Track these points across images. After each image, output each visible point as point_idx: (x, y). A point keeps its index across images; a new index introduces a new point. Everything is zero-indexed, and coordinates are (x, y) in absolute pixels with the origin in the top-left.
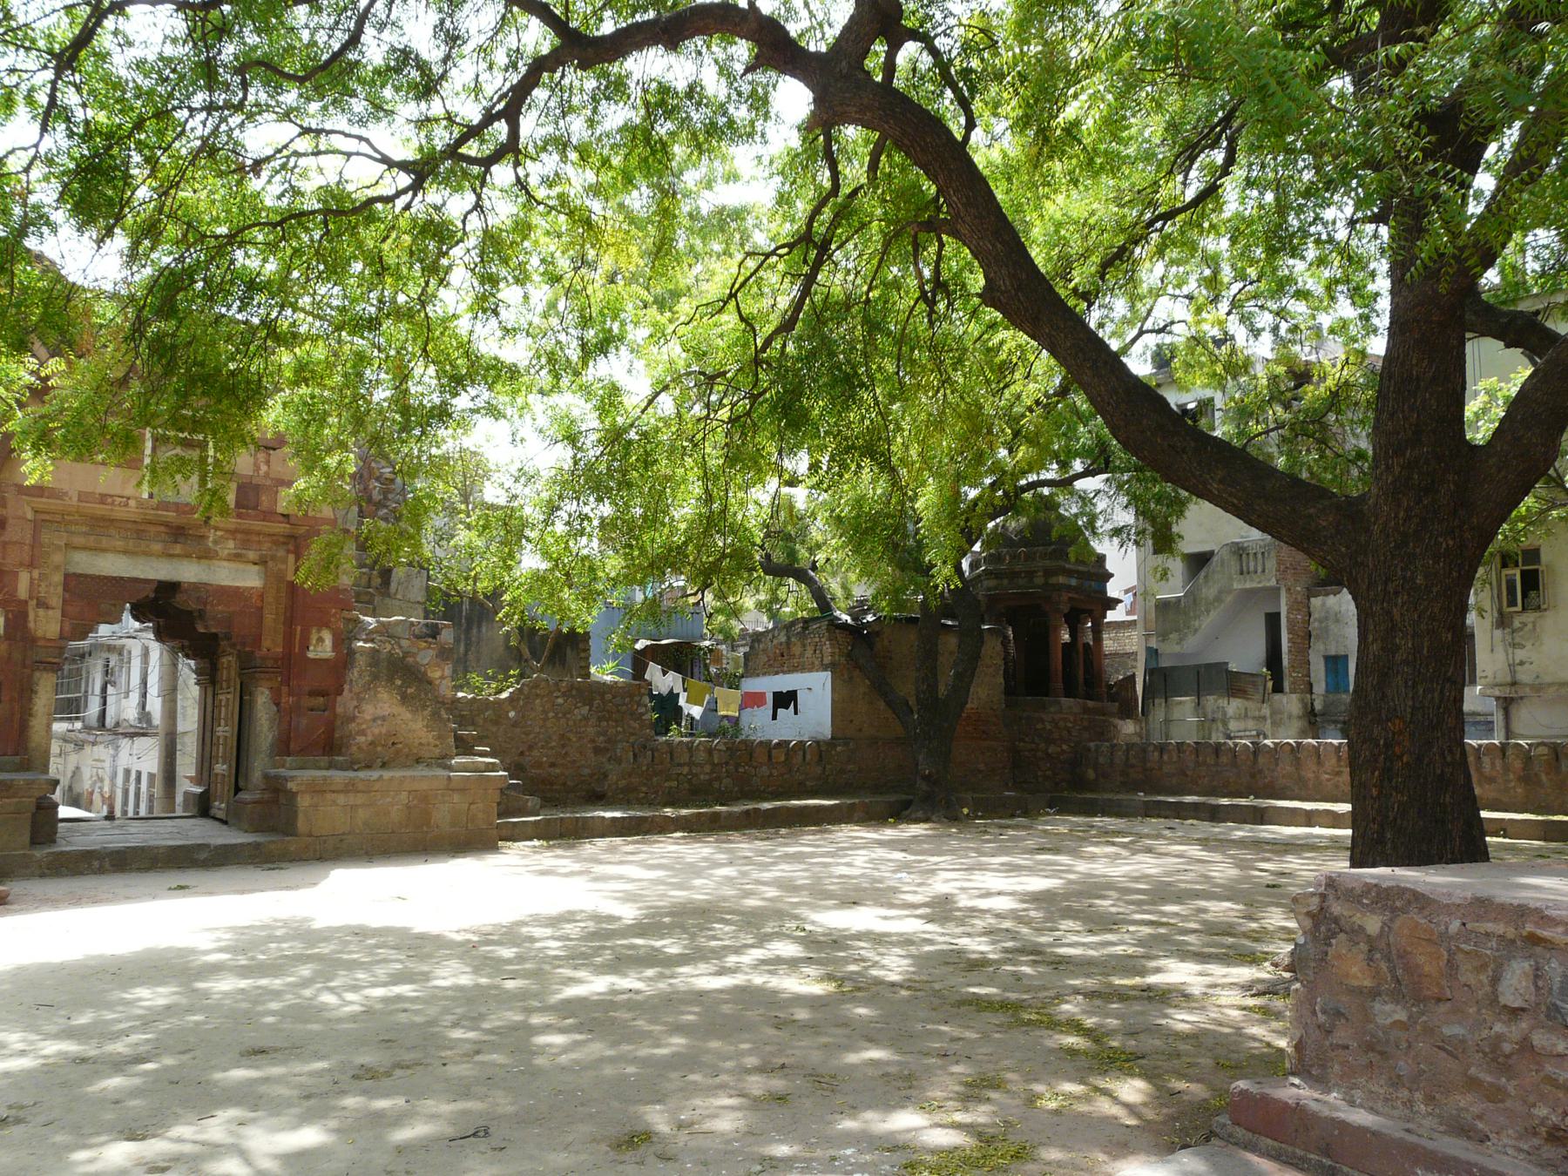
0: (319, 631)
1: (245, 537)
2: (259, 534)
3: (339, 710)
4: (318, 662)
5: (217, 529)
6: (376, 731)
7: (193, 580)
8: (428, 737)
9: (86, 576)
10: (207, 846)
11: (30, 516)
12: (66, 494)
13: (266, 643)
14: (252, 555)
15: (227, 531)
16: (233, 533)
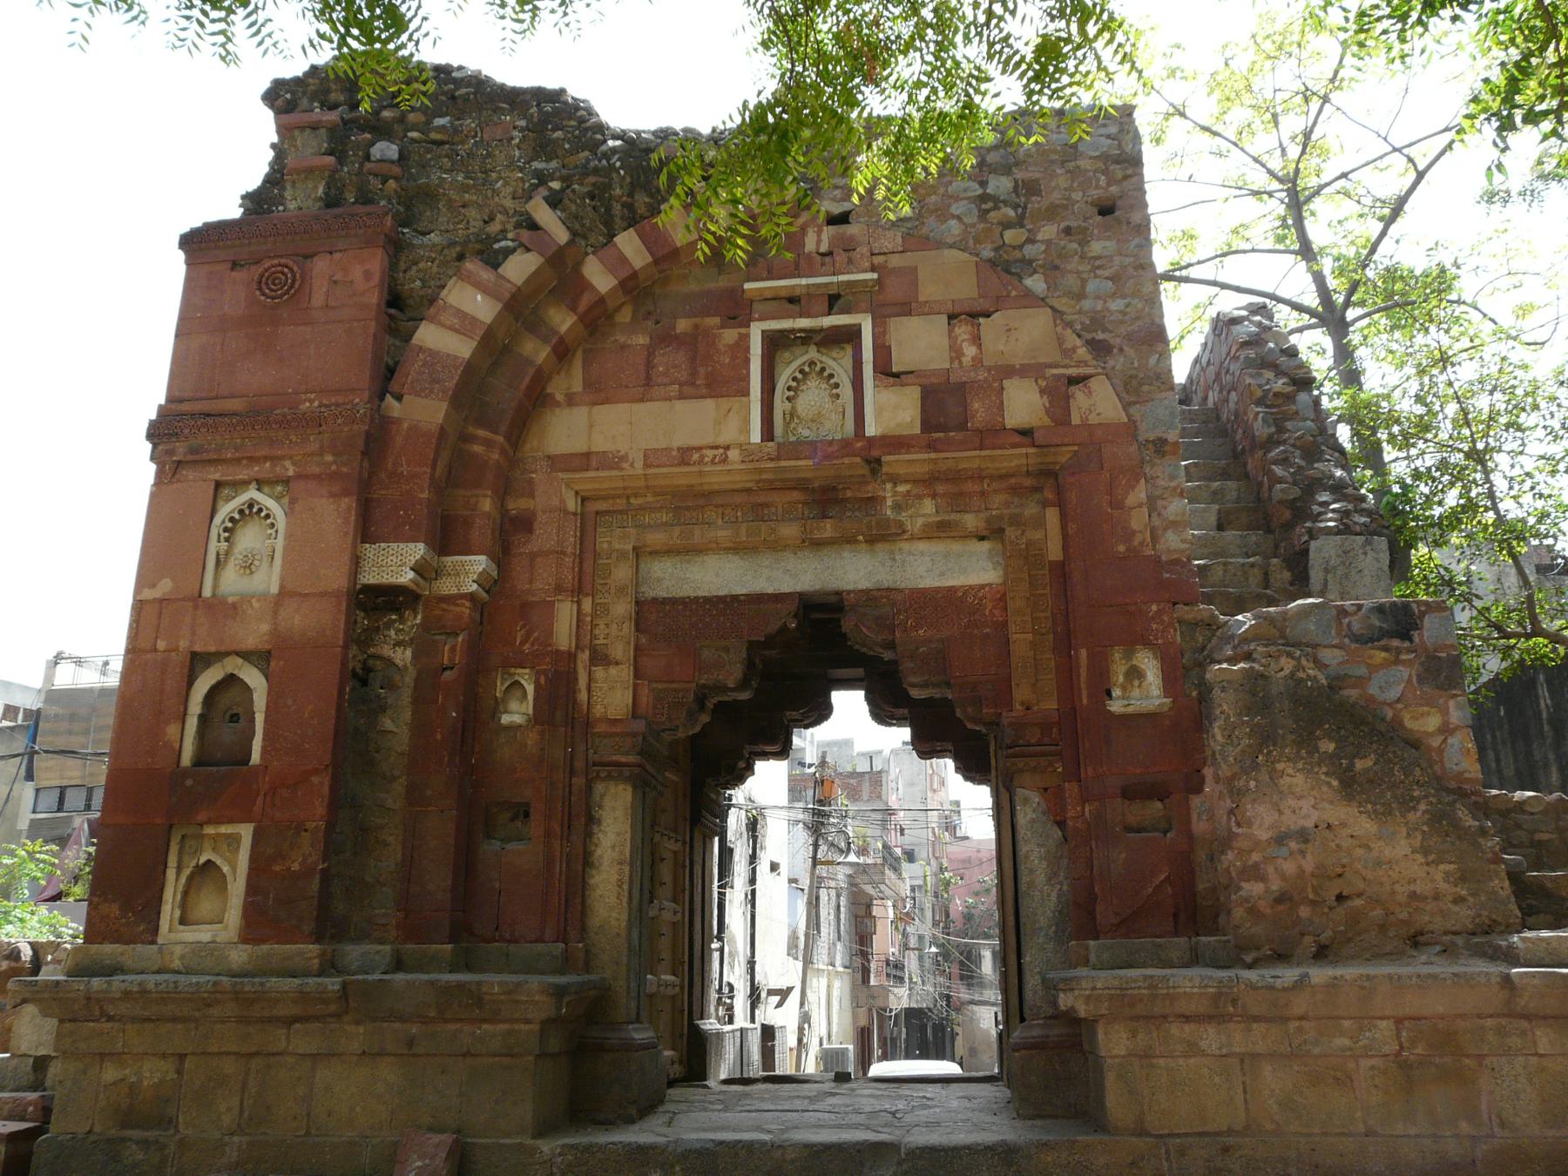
0: (1129, 655)
1: (951, 487)
2: (979, 476)
3: (1199, 826)
4: (1130, 721)
5: (895, 480)
6: (1289, 867)
7: (864, 584)
8: (1437, 878)
9: (672, 601)
10: (891, 1147)
11: (572, 504)
12: (624, 458)
13: (1021, 693)
14: (971, 521)
15: (916, 482)
16: (929, 482)
